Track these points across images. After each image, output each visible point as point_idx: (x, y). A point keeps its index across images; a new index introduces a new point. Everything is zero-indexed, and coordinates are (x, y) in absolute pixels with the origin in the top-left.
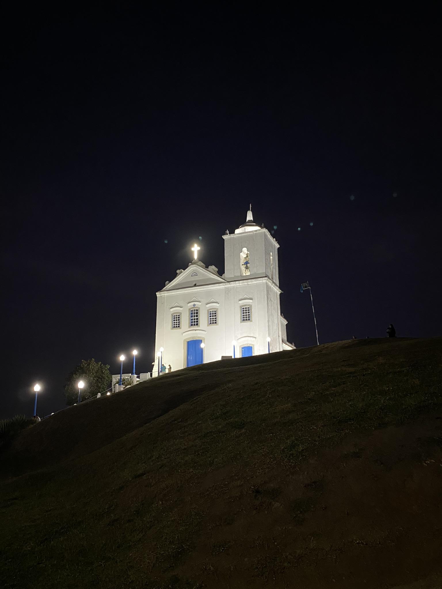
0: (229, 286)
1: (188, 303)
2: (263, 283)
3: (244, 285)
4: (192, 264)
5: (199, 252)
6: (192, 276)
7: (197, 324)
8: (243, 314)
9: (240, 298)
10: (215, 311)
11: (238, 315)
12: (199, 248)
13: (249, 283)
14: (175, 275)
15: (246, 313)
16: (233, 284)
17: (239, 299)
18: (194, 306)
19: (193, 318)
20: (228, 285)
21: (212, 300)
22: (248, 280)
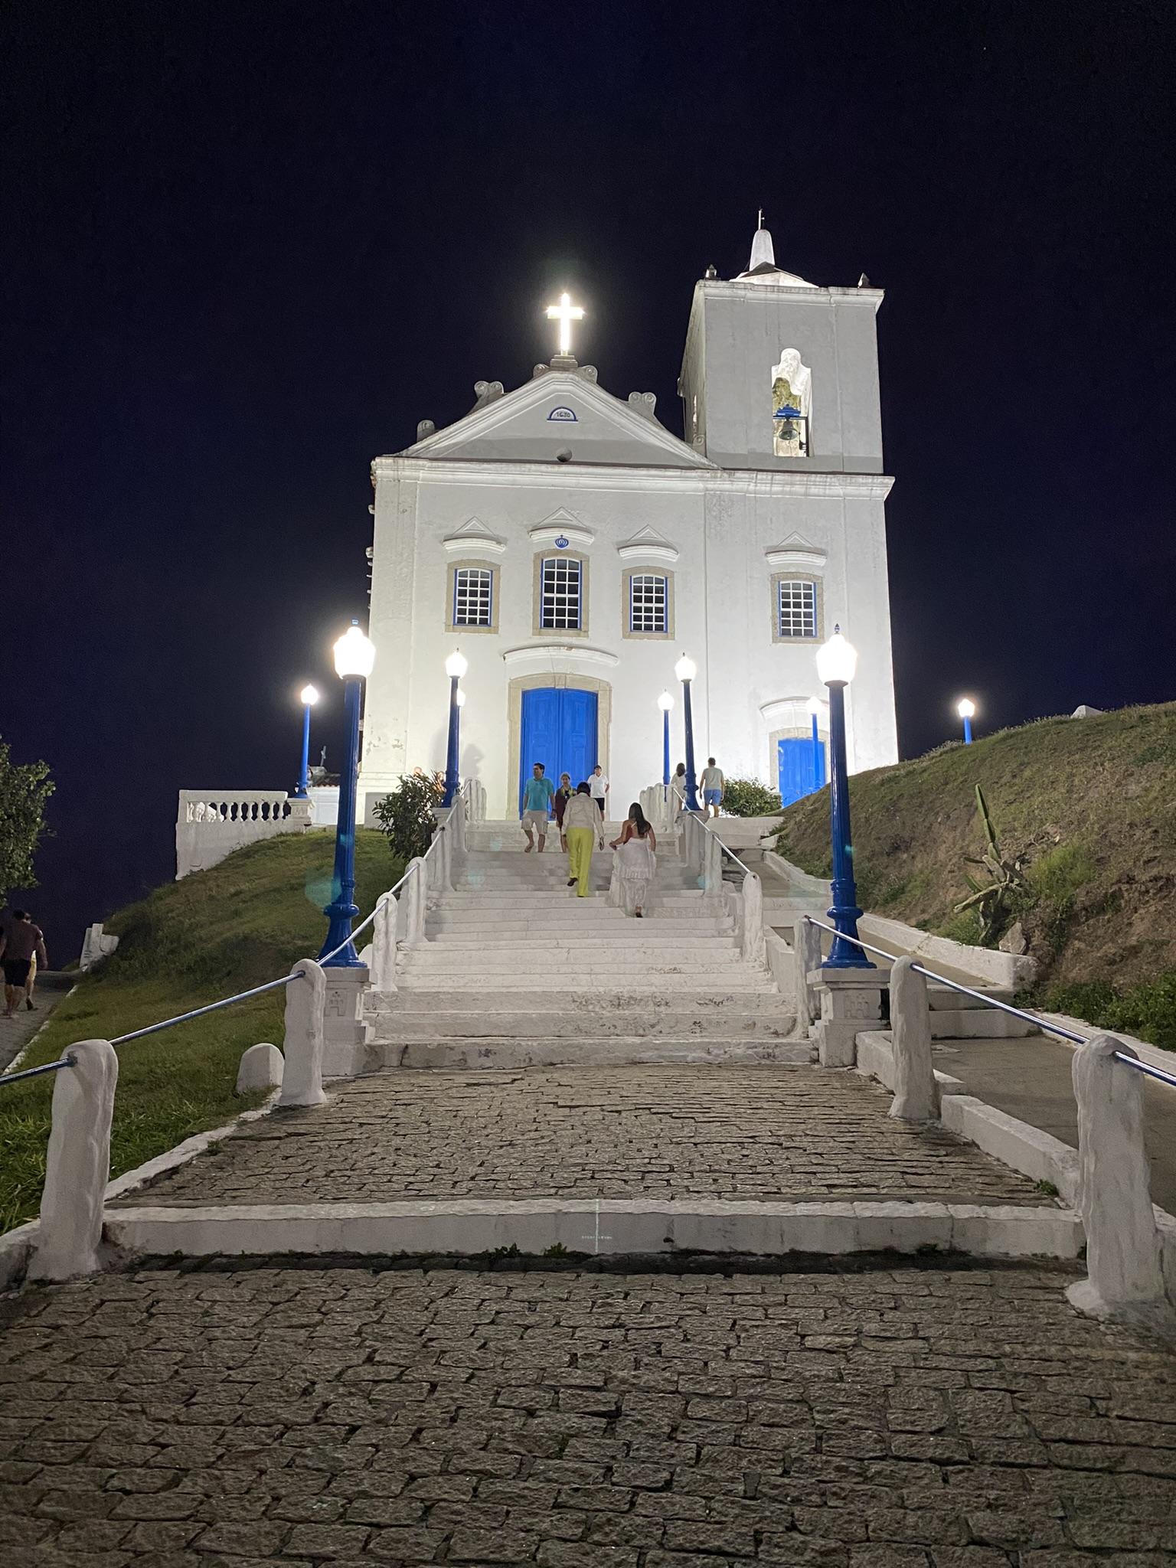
0: (727, 486)
1: (531, 528)
2: (870, 496)
3: (791, 493)
4: (551, 367)
5: (578, 327)
6: (550, 419)
7: (573, 625)
8: (813, 610)
9: (775, 544)
10: (659, 581)
11: (765, 614)
12: (579, 312)
13: (813, 490)
14: (461, 405)
15: (797, 605)
16: (743, 483)
17: (768, 547)
18: (561, 546)
19: (555, 595)
20: (723, 484)
21: (647, 533)
22: (813, 477)
